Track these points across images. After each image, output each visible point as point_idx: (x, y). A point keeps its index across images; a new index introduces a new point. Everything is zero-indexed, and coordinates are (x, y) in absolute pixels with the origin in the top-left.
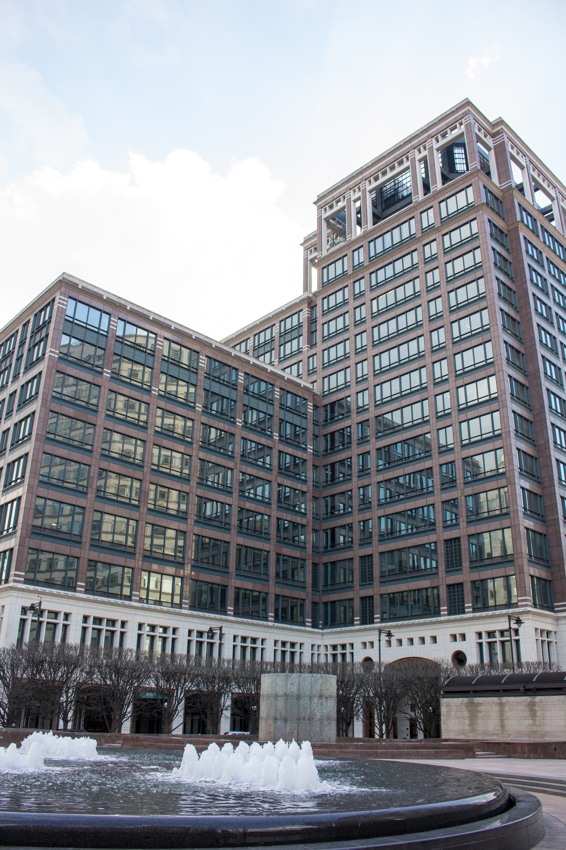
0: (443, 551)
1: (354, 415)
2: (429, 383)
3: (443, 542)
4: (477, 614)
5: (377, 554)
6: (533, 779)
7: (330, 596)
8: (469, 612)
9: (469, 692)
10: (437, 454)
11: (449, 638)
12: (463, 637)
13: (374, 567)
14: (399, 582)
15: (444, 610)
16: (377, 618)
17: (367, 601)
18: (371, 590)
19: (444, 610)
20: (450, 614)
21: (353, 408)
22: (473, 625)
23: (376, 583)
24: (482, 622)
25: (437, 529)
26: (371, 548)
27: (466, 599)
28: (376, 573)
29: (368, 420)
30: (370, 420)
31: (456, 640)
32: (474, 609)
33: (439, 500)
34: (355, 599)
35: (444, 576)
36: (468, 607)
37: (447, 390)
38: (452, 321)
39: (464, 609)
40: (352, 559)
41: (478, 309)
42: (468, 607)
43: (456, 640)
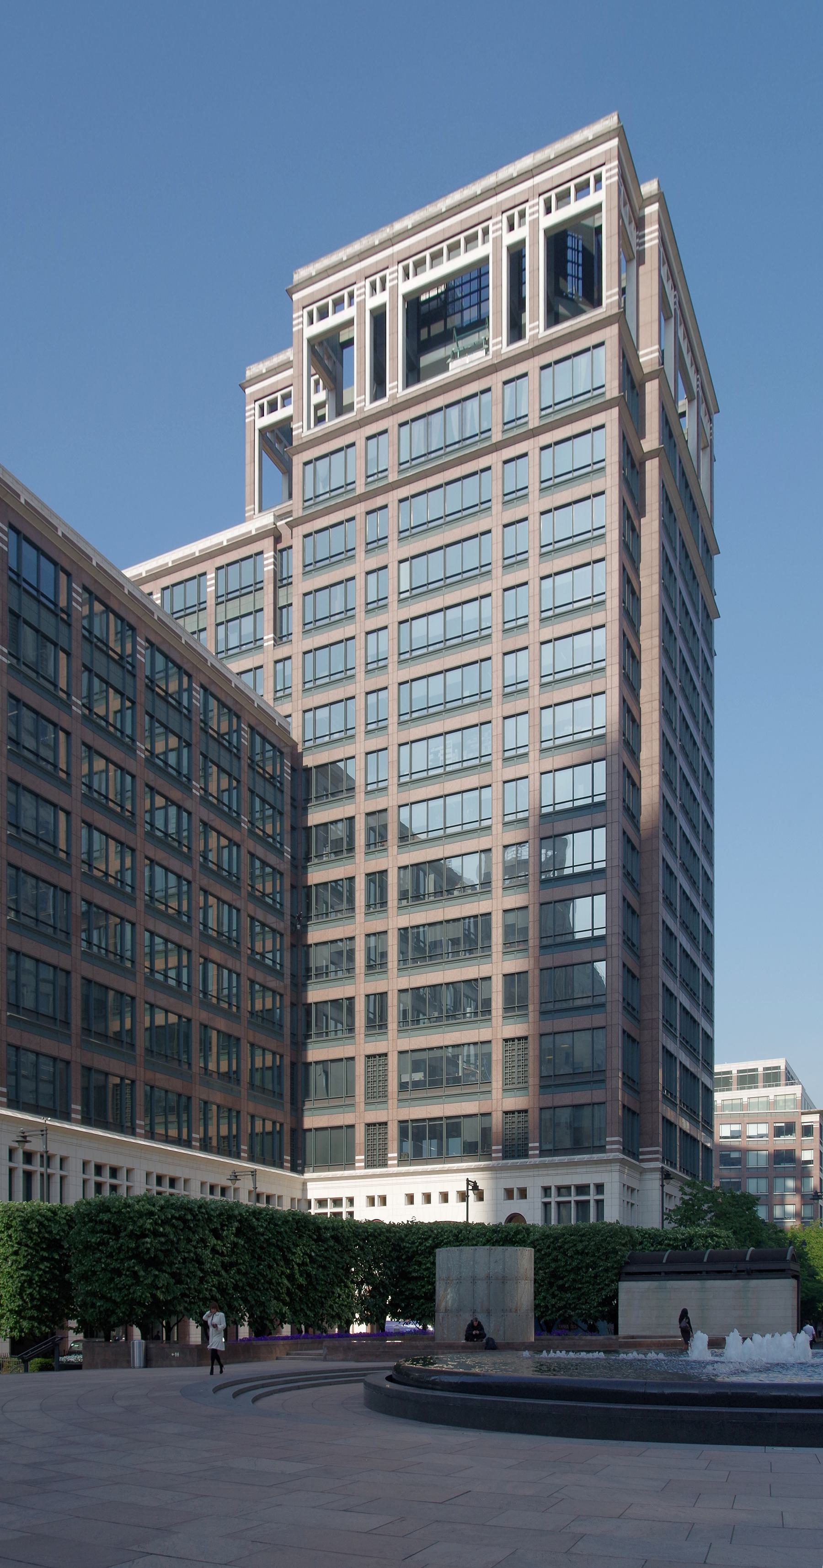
0: (500, 1057)
1: (360, 795)
2: (531, 747)
3: (500, 1042)
4: (547, 1160)
5: (396, 1054)
6: (306, 1373)
7: (315, 1118)
8: (534, 1156)
9: (659, 1273)
10: (500, 890)
11: (403, 1199)
12: (523, 1193)
13: (390, 1074)
14: (429, 1101)
15: (360, 1161)
16: (393, 1159)
17: (376, 1128)
18: (384, 1112)
19: (360, 1161)
20: (367, 1166)
21: (360, 782)
22: (538, 1176)
23: (393, 1101)
24: (551, 1171)
25: (494, 1019)
26: (385, 1043)
27: (390, 1149)
28: (393, 1085)
29: (385, 810)
30: (390, 811)
31: (373, 1204)
32: (541, 1151)
33: (499, 972)
34: (357, 1126)
35: (500, 1097)
36: (534, 1148)
37: (524, 774)
38: (543, 639)
39: (527, 1150)
40: (353, 1059)
41: (588, 626)
42: (534, 1148)
43: (373, 1204)
